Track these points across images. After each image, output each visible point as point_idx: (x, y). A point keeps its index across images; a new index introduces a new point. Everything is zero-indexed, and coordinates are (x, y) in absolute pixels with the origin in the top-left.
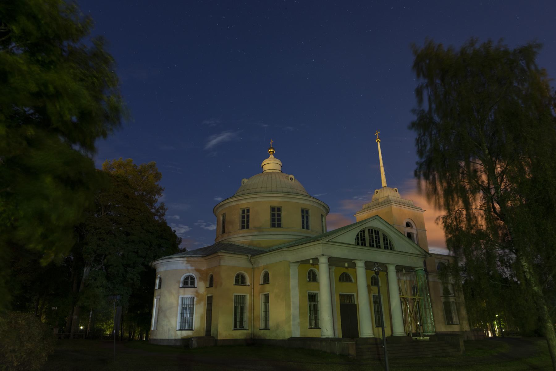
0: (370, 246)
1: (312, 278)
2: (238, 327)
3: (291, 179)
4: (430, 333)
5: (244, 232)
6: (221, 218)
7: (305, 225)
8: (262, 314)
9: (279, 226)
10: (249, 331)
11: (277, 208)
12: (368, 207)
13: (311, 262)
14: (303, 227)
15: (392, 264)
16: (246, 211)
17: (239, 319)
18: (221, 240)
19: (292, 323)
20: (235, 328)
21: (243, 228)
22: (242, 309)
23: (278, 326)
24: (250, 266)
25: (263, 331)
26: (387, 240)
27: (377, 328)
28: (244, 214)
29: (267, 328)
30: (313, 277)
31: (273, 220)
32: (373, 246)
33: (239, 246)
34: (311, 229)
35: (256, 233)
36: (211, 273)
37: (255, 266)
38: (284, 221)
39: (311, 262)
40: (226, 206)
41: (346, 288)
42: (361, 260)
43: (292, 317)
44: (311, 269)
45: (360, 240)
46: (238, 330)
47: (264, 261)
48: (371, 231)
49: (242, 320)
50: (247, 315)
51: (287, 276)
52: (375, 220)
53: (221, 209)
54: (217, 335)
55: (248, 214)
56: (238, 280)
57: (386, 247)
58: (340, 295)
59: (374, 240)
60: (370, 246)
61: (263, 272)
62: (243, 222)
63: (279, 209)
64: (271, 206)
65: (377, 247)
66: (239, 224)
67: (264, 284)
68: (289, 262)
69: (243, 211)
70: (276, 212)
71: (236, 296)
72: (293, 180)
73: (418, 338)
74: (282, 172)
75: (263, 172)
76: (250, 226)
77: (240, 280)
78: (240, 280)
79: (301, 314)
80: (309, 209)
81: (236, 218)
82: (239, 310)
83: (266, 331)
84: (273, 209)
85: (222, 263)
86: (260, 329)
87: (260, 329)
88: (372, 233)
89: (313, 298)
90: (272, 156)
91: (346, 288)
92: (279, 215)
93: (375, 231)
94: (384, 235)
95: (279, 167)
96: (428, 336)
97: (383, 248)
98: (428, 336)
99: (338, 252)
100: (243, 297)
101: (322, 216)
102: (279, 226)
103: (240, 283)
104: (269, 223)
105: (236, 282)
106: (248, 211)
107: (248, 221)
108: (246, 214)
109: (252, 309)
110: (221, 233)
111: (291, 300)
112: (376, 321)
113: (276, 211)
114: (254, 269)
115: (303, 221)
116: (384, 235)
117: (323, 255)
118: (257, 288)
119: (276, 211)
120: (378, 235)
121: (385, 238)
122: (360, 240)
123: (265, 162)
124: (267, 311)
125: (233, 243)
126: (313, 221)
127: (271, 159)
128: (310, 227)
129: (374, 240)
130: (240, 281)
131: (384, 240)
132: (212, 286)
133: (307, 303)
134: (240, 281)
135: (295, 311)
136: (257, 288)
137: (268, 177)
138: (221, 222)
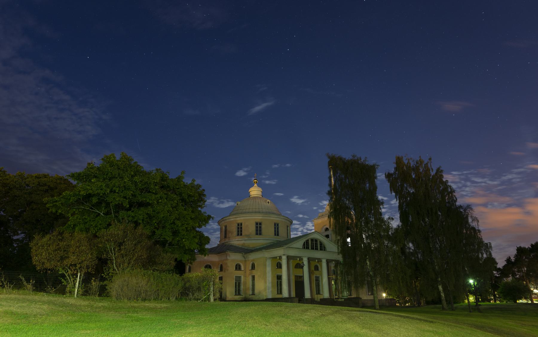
0: (312, 249)
1: (279, 266)
2: (237, 293)
3: (268, 202)
4: (345, 297)
5: (239, 238)
6: (224, 228)
7: (277, 233)
8: (251, 287)
9: (260, 234)
10: (243, 296)
11: (259, 223)
12: (322, 216)
13: (278, 258)
14: (275, 235)
15: (324, 258)
16: (240, 224)
17: (237, 290)
18: (224, 242)
19: (267, 291)
20: (236, 295)
21: (238, 235)
22: (239, 284)
23: (260, 293)
24: (244, 259)
25: (251, 296)
26: (322, 245)
27: (317, 295)
28: (239, 227)
29: (253, 294)
30: (279, 266)
31: (257, 230)
32: (313, 249)
33: (235, 246)
34: (280, 236)
35: (246, 239)
36: (221, 263)
37: (247, 259)
38: (263, 231)
39: (278, 258)
40: (228, 221)
41: (298, 272)
42: (305, 257)
43: (267, 288)
44: (278, 261)
45: (306, 246)
46: (237, 295)
47: (252, 257)
48: (312, 240)
49: (239, 290)
50: (242, 287)
51: (265, 265)
52: (315, 234)
53: (223, 222)
54: (226, 298)
55: (241, 226)
56: (237, 267)
57: (321, 249)
58: (295, 276)
59: (314, 245)
60: (312, 249)
61: (251, 262)
62: (238, 231)
63: (260, 224)
64: (255, 222)
65: (316, 249)
66: (235, 233)
67: (252, 270)
68: (266, 258)
69: (238, 225)
70: (259, 226)
71: (236, 276)
72: (270, 203)
73: (338, 300)
74: (262, 196)
75: (249, 197)
76: (243, 234)
77: (238, 267)
78: (238, 267)
79: (273, 286)
80: (279, 223)
81: (233, 229)
82: (237, 284)
83: (253, 296)
84: (257, 224)
85: (228, 257)
86: (250, 295)
87: (250, 295)
88: (313, 241)
89: (279, 278)
90: (256, 185)
91: (298, 272)
92: (260, 227)
93: (315, 240)
94: (320, 242)
95: (260, 193)
96: (343, 299)
97: (320, 250)
98: (343, 299)
99: (292, 253)
100: (240, 277)
101: (287, 227)
102: (260, 234)
103: (238, 269)
104: (254, 232)
105: (236, 269)
106: (241, 224)
107: (241, 231)
108: (240, 227)
109: (245, 283)
110: (224, 238)
111: (267, 278)
112: (316, 291)
113: (259, 227)
114: (246, 261)
115: (275, 231)
116: (320, 242)
117: (284, 255)
118: (248, 272)
119: (259, 227)
120: (317, 242)
121: (321, 244)
122: (306, 246)
123: (251, 189)
124: (253, 285)
125: (232, 244)
126: (282, 230)
127: (255, 187)
128: (280, 235)
129: (314, 245)
130: (238, 268)
131: (320, 245)
132: (222, 271)
133: (276, 280)
134: (238, 268)
135: (269, 284)
136: (248, 272)
137: (253, 201)
138: (224, 230)
